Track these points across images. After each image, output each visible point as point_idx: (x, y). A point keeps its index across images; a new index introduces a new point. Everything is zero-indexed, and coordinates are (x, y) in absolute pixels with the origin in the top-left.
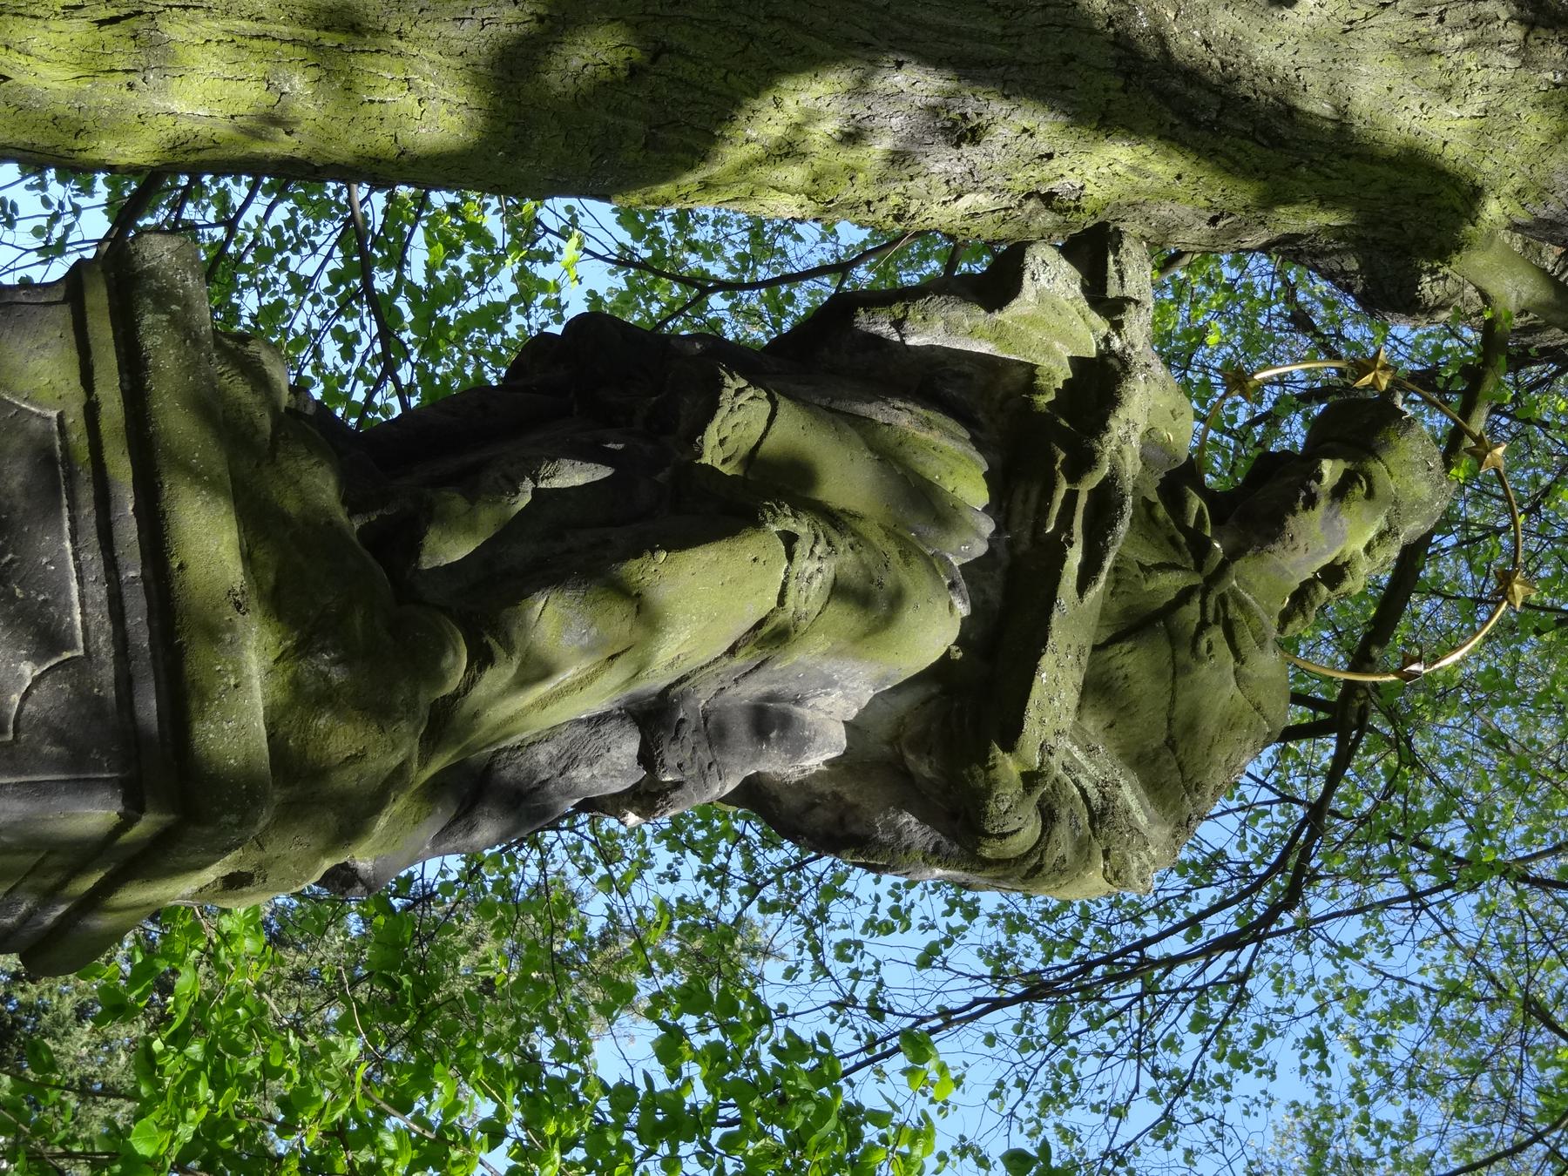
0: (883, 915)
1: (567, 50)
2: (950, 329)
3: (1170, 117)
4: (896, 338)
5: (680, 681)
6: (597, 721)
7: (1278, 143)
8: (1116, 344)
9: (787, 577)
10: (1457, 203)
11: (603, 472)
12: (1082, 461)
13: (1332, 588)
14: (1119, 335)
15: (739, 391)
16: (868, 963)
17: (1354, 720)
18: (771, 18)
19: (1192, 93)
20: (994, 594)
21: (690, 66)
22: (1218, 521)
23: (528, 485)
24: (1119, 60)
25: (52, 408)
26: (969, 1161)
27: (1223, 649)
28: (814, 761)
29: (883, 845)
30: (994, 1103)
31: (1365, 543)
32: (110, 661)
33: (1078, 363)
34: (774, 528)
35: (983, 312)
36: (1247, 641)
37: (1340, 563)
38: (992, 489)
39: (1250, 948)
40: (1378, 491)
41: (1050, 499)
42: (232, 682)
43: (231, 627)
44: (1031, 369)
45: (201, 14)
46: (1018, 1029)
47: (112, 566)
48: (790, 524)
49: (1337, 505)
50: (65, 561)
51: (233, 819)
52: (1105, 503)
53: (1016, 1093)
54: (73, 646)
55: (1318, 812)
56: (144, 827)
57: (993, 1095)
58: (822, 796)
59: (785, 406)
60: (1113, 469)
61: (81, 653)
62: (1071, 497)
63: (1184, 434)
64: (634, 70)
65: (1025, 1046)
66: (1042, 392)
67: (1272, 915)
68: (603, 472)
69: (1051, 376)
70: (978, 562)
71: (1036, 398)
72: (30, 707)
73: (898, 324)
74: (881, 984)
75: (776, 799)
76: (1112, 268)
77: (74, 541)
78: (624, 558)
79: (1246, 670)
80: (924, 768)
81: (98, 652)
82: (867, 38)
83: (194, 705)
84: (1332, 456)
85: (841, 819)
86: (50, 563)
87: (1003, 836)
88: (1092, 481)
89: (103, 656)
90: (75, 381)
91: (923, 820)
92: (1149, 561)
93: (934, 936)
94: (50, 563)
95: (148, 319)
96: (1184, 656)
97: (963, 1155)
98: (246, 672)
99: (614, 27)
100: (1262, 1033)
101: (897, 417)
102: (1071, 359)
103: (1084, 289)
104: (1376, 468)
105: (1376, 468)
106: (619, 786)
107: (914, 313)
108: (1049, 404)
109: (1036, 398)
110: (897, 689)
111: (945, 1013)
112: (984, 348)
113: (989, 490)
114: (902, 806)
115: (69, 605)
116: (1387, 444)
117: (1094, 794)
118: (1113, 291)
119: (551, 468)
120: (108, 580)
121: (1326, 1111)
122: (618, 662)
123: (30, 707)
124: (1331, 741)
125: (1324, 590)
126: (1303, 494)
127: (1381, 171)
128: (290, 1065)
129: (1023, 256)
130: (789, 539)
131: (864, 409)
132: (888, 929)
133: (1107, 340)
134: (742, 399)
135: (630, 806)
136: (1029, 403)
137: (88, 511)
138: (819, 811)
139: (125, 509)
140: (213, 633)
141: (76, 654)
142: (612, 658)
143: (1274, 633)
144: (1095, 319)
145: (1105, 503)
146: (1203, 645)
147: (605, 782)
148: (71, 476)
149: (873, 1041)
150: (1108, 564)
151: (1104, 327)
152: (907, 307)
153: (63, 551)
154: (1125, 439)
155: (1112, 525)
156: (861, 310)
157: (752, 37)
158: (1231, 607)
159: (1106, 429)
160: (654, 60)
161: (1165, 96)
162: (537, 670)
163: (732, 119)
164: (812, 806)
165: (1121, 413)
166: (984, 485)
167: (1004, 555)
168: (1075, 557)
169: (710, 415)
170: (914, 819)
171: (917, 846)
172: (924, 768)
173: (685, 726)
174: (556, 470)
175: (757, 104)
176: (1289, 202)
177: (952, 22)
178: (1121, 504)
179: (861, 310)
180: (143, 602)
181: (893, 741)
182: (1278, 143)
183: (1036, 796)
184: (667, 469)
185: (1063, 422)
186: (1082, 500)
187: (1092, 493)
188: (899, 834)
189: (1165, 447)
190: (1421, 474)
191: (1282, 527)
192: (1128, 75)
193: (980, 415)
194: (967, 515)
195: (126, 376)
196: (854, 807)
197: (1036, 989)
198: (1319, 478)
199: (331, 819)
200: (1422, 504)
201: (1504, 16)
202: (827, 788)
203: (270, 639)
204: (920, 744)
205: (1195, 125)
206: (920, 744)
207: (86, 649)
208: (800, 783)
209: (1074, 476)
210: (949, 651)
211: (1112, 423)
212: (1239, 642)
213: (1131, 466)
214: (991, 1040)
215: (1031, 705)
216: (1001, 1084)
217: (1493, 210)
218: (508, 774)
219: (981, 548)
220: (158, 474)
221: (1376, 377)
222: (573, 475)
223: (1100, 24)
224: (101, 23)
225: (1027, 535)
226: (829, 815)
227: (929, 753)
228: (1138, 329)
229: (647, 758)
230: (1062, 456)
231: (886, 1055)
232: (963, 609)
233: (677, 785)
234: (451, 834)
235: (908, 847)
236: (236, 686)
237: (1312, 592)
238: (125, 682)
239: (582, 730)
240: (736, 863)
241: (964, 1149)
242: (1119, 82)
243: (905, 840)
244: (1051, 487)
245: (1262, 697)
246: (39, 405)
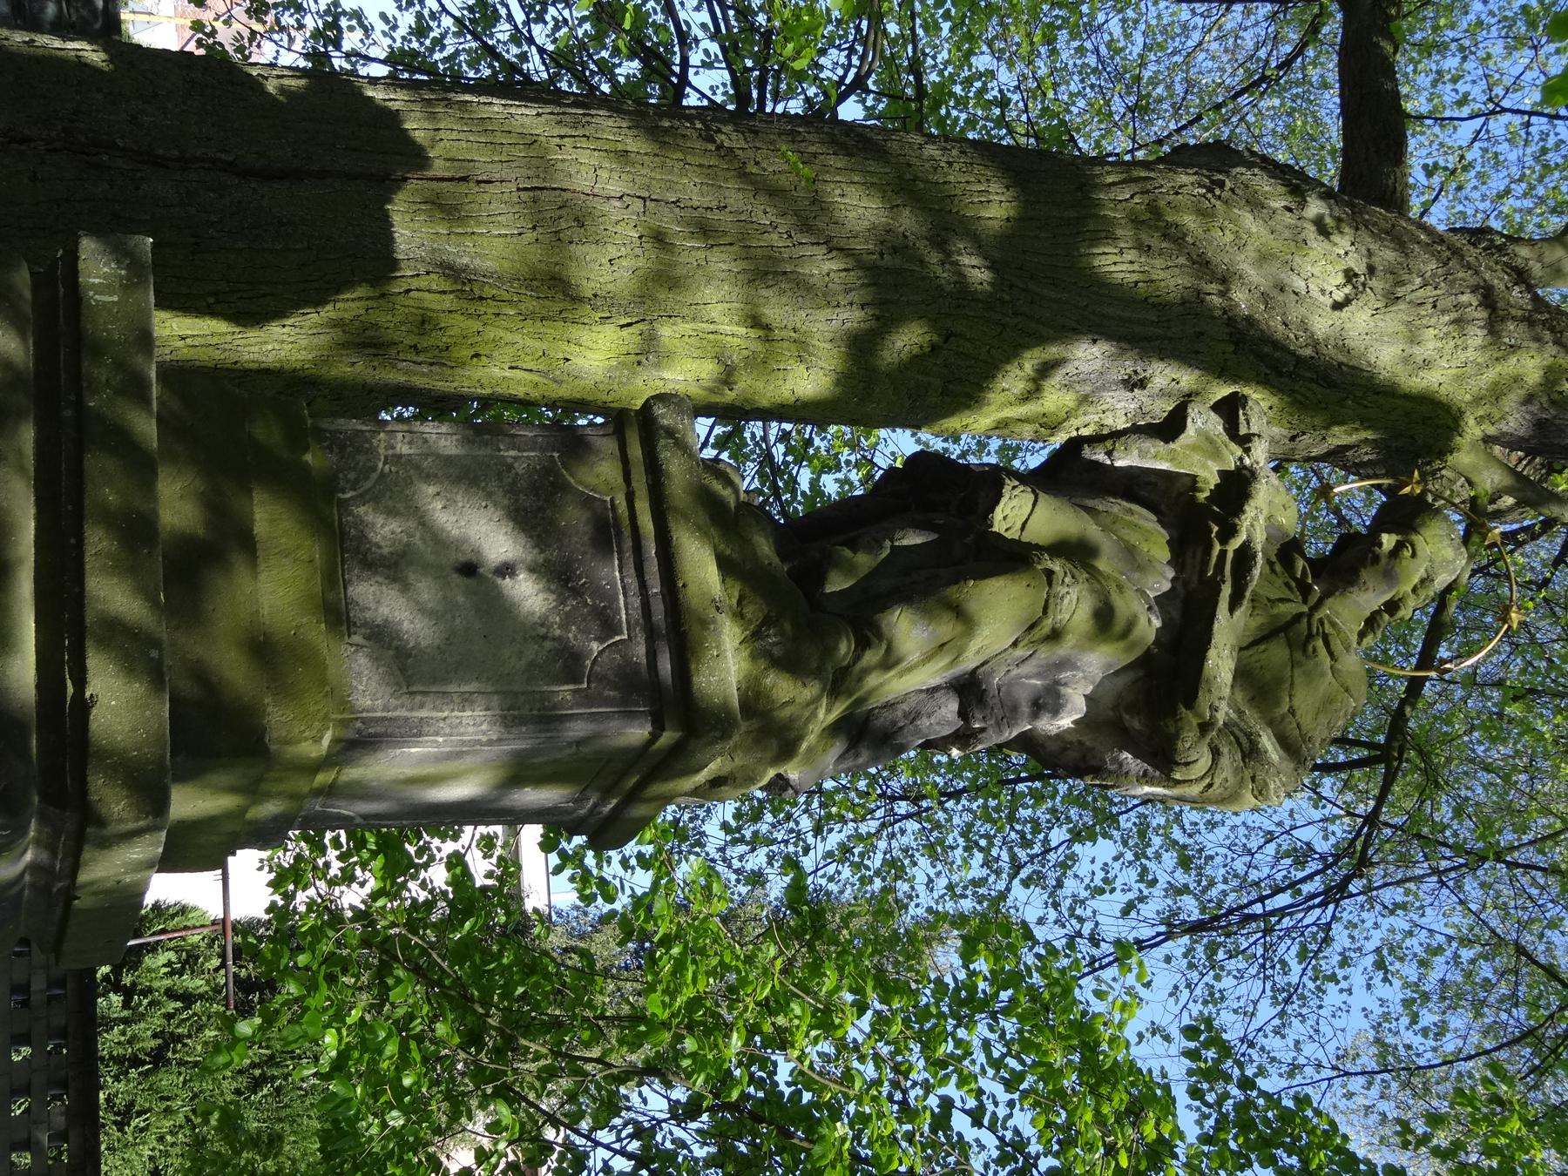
0: (1098, 882)
1: (894, 337)
2: (1142, 455)
3: (1265, 370)
5: (983, 664)
6: (932, 691)
7: (1332, 385)
8: (1247, 461)
10: (1450, 422)
11: (932, 537)
12: (1229, 532)
13: (1391, 615)
15: (1014, 488)
16: (1089, 912)
18: (1016, 314)
19: (1277, 354)
20: (1176, 614)
21: (968, 345)
22: (1316, 576)
23: (888, 543)
24: (1231, 335)
26: (1158, 1037)
27: (1322, 651)
28: (1066, 722)
29: (1110, 772)
30: (1172, 1000)
33: (1222, 474)
36: (1337, 645)
38: (1171, 551)
39: (1331, 907)
40: (1419, 553)
43: (714, 621)
44: (1194, 478)
45: (679, 320)
46: (1185, 956)
47: (643, 586)
51: (717, 734)
52: (1245, 556)
53: (1186, 993)
54: (621, 633)
55: (1372, 819)
56: (668, 737)
57: (1171, 995)
58: (1071, 743)
62: (1223, 554)
63: (1288, 520)
64: (934, 348)
65: (1191, 966)
66: (1201, 491)
67: (1347, 880)
68: (932, 537)
69: (1206, 482)
72: (597, 668)
73: (1109, 453)
74: (1097, 924)
75: (1043, 746)
76: (1242, 418)
77: (621, 572)
80: (1136, 724)
82: (1074, 325)
83: (693, 666)
84: (1389, 532)
85: (1084, 758)
87: (1187, 764)
88: (1235, 543)
90: (620, 480)
91: (1136, 756)
92: (1273, 596)
93: (1131, 896)
95: (662, 442)
96: (1298, 656)
97: (1153, 1034)
99: (921, 322)
100: (1345, 962)
103: (1225, 429)
104: (1417, 539)
105: (1417, 539)
106: (947, 731)
107: (1119, 446)
110: (1117, 673)
111: (1138, 942)
112: (1164, 466)
114: (1122, 748)
115: (619, 609)
116: (1423, 524)
118: (1243, 431)
121: (1386, 1017)
123: (597, 668)
124: (1381, 768)
125: (1386, 617)
127: (1399, 402)
128: (740, 964)
131: (1090, 503)
132: (1101, 891)
133: (1241, 459)
134: (1016, 492)
135: (953, 744)
136: (1194, 497)
137: (628, 555)
140: (704, 623)
143: (1355, 645)
144: (1233, 446)
146: (1310, 648)
147: (938, 728)
148: (619, 534)
149: (1093, 960)
150: (1248, 594)
151: (1239, 452)
154: (1256, 518)
155: (1249, 570)
157: (1004, 326)
158: (1327, 626)
159: (1243, 512)
160: (946, 341)
161: (1261, 357)
162: (889, 662)
163: (994, 377)
164: (1066, 749)
165: (1252, 503)
166: (1167, 548)
168: (1226, 590)
169: (997, 502)
172: (1136, 724)
175: (1008, 367)
176: (1341, 423)
177: (1127, 314)
180: (661, 607)
181: (1116, 707)
182: (1332, 385)
183: (1208, 739)
186: (1230, 556)
187: (1236, 551)
188: (1121, 765)
189: (1280, 527)
190: (1446, 542)
191: (1358, 576)
192: (1236, 344)
193: (1163, 507)
194: (1157, 565)
196: (1091, 750)
197: (1195, 928)
198: (1380, 545)
199: (774, 744)
200: (1448, 562)
201: (1475, 303)
202: (1074, 738)
203: (737, 630)
204: (1132, 708)
205: (1280, 374)
206: (1132, 708)
208: (1057, 735)
211: (1246, 508)
213: (1259, 539)
214: (1168, 959)
216: (1176, 987)
217: (1473, 429)
218: (879, 723)
219: (1167, 586)
222: (913, 539)
223: (1218, 313)
224: (622, 326)
225: (1195, 578)
228: (1260, 454)
229: (963, 714)
230: (1216, 529)
231: (1102, 968)
233: (983, 730)
238: (652, 655)
239: (923, 696)
240: (1005, 856)
241: (1155, 1030)
242: (1231, 348)
243: (1125, 769)
244: (1210, 547)
245: (1349, 682)
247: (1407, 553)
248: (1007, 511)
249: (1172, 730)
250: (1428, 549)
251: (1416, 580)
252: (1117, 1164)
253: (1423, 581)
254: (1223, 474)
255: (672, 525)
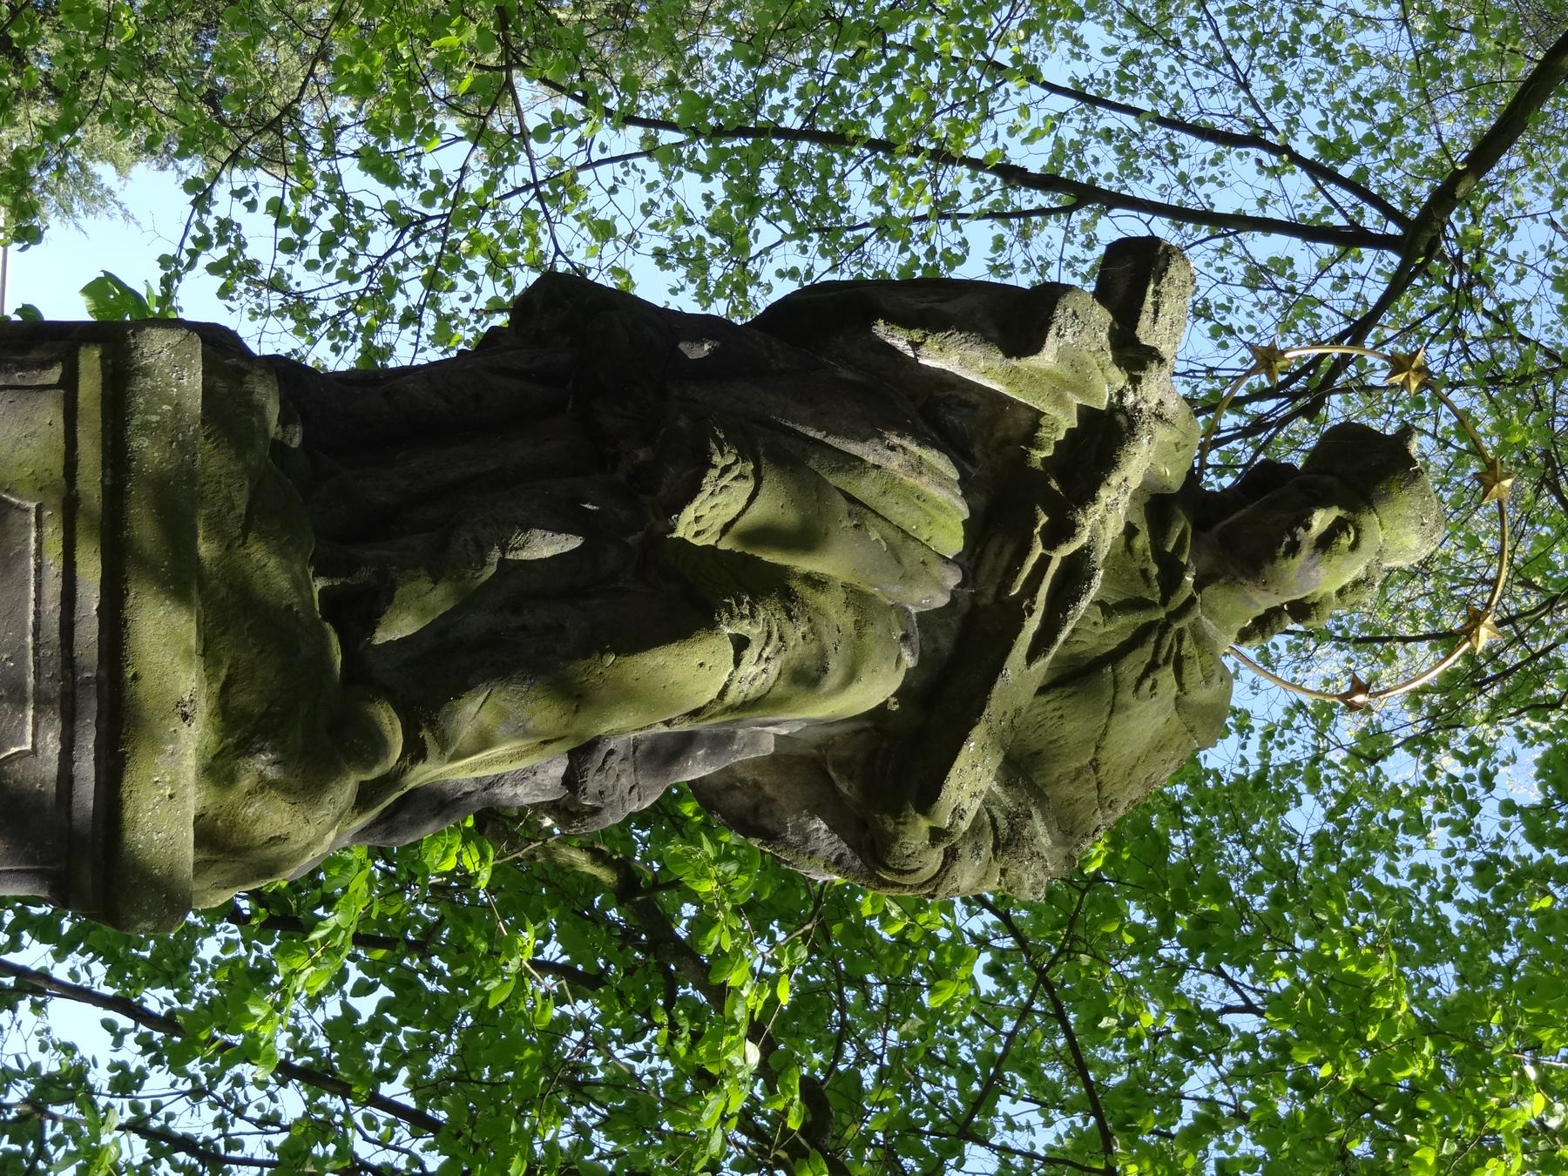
4: (911, 354)
9: (730, 680)
11: (574, 542)
12: (1061, 531)
14: (1135, 390)
17: (1422, 249)
23: (495, 555)
25: (31, 499)
29: (789, 845)
31: (1339, 586)
32: (55, 757)
33: (1086, 414)
34: (728, 631)
35: (1001, 356)
37: (1309, 602)
38: (967, 538)
41: (1022, 564)
42: (168, 792)
48: (744, 628)
49: (1319, 555)
50: (25, 657)
58: (743, 781)
59: (771, 479)
60: (1091, 539)
61: (29, 747)
62: (1044, 562)
70: (938, 612)
71: (1033, 452)
76: (1149, 299)
78: (571, 658)
79: (1188, 698)
81: (44, 749)
85: (755, 810)
86: (10, 659)
88: (1067, 549)
89: (49, 753)
91: (833, 828)
94: (10, 659)
98: (183, 782)
101: (888, 459)
102: (1080, 407)
108: (1045, 460)
109: (1033, 452)
113: (966, 538)
114: (816, 810)
116: (1386, 496)
117: (1003, 823)
119: (521, 538)
120: (64, 678)
122: (549, 748)
126: (1288, 539)
129: (1052, 308)
130: (741, 644)
133: (1121, 394)
136: (1025, 456)
138: (737, 794)
139: (89, 609)
141: (24, 748)
142: (545, 743)
145: (1075, 573)
152: (926, 336)
153: (24, 647)
155: (1076, 599)
156: (881, 322)
159: (1094, 500)
167: (965, 605)
168: (1032, 624)
169: (690, 499)
170: (824, 826)
171: (822, 854)
173: (614, 757)
174: (526, 542)
178: (1091, 577)
179: (881, 322)
184: (640, 534)
185: (1054, 484)
186: (1054, 566)
188: (806, 839)
193: (977, 450)
195: (108, 471)
196: (770, 800)
198: (1308, 527)
202: (750, 776)
204: (843, 765)
206: (843, 765)
207: (34, 745)
209: (1052, 541)
210: (887, 702)
212: (1186, 678)
215: (953, 773)
219: (942, 600)
220: (126, 581)
221: (1408, 377)
222: (545, 546)
225: (991, 591)
226: (746, 800)
227: (850, 778)
232: (909, 660)
234: (370, 835)
235: (812, 853)
236: (171, 797)
237: (1275, 621)
238: (66, 777)
243: (811, 846)
244: (1026, 550)
246: (20, 497)
247: (1346, 541)
248: (704, 511)
249: (890, 829)
250: (1381, 536)
251: (1347, 580)
252: (774, 994)
253: (1357, 583)
254: (1088, 415)
255: (131, 571)
